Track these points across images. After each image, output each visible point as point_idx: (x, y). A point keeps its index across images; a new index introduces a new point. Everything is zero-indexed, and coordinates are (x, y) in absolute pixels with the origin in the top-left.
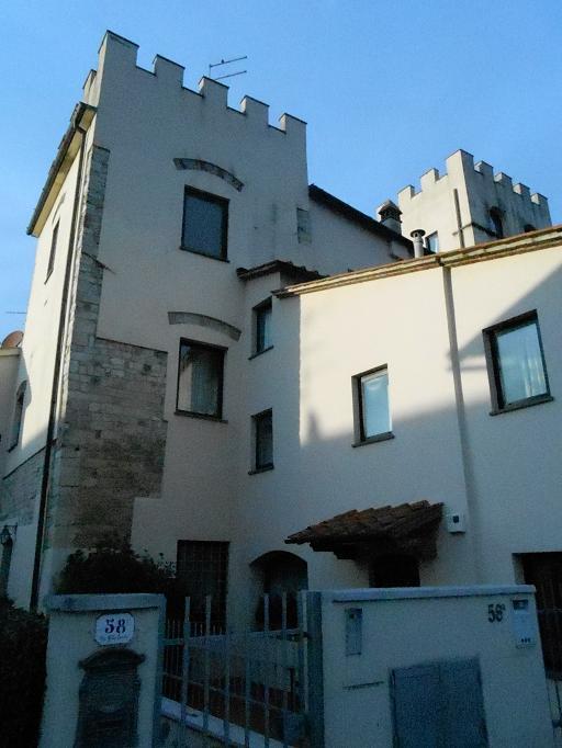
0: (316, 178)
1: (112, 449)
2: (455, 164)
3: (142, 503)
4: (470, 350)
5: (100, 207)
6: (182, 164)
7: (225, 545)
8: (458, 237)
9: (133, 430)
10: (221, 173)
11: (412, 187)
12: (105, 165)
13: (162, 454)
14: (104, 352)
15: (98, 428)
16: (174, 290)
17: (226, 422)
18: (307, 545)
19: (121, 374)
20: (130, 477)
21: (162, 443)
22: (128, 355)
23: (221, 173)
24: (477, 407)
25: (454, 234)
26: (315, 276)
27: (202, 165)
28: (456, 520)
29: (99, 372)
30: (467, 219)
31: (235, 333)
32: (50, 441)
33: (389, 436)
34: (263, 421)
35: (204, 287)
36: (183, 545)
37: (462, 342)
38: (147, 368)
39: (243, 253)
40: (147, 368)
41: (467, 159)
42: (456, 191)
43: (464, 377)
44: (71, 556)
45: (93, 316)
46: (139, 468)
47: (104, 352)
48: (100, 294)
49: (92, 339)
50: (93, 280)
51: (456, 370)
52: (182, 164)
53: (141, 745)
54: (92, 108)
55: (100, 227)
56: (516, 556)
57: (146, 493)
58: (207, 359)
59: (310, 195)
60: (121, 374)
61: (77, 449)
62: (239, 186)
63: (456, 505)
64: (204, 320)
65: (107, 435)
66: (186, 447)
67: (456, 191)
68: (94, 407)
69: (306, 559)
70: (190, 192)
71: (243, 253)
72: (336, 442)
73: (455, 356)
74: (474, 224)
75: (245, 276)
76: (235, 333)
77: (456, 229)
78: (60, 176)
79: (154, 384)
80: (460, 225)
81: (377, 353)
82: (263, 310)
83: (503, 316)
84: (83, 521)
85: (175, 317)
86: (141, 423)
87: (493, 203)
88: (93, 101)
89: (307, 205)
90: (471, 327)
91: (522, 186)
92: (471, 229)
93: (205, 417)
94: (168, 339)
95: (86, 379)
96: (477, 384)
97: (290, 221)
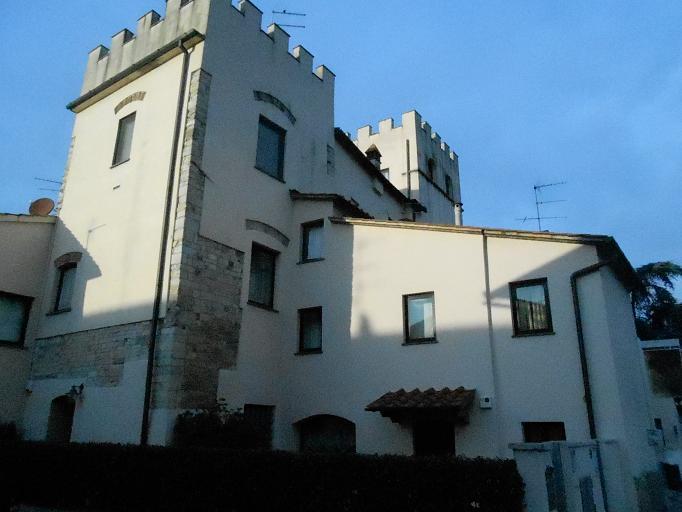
0: (339, 122)
1: (206, 329)
2: (409, 119)
3: (223, 373)
4: (499, 293)
5: (203, 124)
6: (259, 95)
7: (272, 408)
8: (406, 177)
9: (219, 315)
10: (282, 108)
11: (371, 127)
12: (208, 88)
13: (238, 334)
14: (204, 248)
15: (198, 311)
16: (252, 204)
17: (277, 312)
18: (378, 413)
19: (214, 267)
20: (217, 351)
21: (237, 326)
22: (218, 252)
23: (282, 108)
24: (502, 330)
25: (404, 174)
26: (366, 216)
27: (271, 99)
28: (487, 400)
29: (201, 265)
30: (414, 165)
31: (286, 241)
32: (156, 321)
33: (433, 340)
34: (311, 318)
35: (265, 199)
36: (246, 406)
37: (492, 289)
38: (231, 264)
39: (293, 180)
40: (231, 264)
41: (418, 117)
42: (408, 141)
43: (493, 309)
44: (180, 416)
45: (197, 217)
46: (222, 345)
47: (204, 248)
48: (202, 198)
49: (196, 237)
50: (198, 186)
51: (489, 304)
52: (259, 95)
53: (530, 509)
54: (201, 36)
55: (203, 142)
56: (523, 423)
57: (228, 365)
58: (264, 259)
59: (335, 135)
60: (214, 267)
61: (184, 328)
62: (293, 120)
63: (485, 392)
64: (267, 228)
65: (205, 317)
66: (253, 326)
67: (408, 141)
68: (196, 294)
69: (354, 421)
70: (263, 120)
71: (293, 180)
72: (384, 340)
73: (489, 296)
74: (419, 170)
75: (295, 196)
76: (286, 241)
77: (406, 171)
78: (136, 74)
79: (235, 278)
80: (409, 169)
81: (418, 283)
82: (309, 227)
83: (527, 276)
84: (187, 387)
85: (250, 224)
86: (226, 309)
87: (430, 156)
88: (202, 30)
89: (333, 143)
90: (501, 278)
91: (446, 144)
92: (417, 174)
93: (259, 305)
94: (244, 241)
95: (192, 270)
96: (503, 316)
97: (323, 156)
